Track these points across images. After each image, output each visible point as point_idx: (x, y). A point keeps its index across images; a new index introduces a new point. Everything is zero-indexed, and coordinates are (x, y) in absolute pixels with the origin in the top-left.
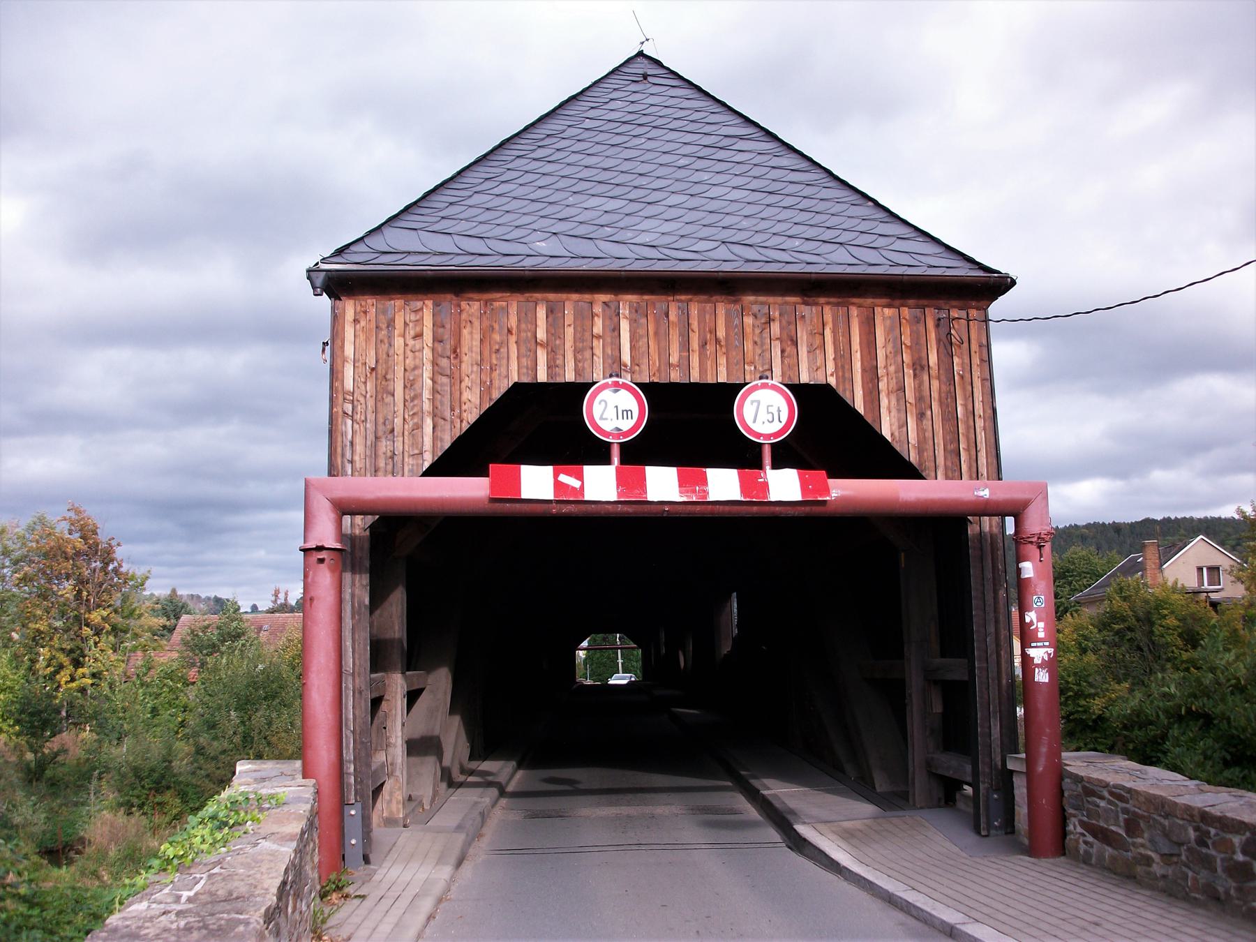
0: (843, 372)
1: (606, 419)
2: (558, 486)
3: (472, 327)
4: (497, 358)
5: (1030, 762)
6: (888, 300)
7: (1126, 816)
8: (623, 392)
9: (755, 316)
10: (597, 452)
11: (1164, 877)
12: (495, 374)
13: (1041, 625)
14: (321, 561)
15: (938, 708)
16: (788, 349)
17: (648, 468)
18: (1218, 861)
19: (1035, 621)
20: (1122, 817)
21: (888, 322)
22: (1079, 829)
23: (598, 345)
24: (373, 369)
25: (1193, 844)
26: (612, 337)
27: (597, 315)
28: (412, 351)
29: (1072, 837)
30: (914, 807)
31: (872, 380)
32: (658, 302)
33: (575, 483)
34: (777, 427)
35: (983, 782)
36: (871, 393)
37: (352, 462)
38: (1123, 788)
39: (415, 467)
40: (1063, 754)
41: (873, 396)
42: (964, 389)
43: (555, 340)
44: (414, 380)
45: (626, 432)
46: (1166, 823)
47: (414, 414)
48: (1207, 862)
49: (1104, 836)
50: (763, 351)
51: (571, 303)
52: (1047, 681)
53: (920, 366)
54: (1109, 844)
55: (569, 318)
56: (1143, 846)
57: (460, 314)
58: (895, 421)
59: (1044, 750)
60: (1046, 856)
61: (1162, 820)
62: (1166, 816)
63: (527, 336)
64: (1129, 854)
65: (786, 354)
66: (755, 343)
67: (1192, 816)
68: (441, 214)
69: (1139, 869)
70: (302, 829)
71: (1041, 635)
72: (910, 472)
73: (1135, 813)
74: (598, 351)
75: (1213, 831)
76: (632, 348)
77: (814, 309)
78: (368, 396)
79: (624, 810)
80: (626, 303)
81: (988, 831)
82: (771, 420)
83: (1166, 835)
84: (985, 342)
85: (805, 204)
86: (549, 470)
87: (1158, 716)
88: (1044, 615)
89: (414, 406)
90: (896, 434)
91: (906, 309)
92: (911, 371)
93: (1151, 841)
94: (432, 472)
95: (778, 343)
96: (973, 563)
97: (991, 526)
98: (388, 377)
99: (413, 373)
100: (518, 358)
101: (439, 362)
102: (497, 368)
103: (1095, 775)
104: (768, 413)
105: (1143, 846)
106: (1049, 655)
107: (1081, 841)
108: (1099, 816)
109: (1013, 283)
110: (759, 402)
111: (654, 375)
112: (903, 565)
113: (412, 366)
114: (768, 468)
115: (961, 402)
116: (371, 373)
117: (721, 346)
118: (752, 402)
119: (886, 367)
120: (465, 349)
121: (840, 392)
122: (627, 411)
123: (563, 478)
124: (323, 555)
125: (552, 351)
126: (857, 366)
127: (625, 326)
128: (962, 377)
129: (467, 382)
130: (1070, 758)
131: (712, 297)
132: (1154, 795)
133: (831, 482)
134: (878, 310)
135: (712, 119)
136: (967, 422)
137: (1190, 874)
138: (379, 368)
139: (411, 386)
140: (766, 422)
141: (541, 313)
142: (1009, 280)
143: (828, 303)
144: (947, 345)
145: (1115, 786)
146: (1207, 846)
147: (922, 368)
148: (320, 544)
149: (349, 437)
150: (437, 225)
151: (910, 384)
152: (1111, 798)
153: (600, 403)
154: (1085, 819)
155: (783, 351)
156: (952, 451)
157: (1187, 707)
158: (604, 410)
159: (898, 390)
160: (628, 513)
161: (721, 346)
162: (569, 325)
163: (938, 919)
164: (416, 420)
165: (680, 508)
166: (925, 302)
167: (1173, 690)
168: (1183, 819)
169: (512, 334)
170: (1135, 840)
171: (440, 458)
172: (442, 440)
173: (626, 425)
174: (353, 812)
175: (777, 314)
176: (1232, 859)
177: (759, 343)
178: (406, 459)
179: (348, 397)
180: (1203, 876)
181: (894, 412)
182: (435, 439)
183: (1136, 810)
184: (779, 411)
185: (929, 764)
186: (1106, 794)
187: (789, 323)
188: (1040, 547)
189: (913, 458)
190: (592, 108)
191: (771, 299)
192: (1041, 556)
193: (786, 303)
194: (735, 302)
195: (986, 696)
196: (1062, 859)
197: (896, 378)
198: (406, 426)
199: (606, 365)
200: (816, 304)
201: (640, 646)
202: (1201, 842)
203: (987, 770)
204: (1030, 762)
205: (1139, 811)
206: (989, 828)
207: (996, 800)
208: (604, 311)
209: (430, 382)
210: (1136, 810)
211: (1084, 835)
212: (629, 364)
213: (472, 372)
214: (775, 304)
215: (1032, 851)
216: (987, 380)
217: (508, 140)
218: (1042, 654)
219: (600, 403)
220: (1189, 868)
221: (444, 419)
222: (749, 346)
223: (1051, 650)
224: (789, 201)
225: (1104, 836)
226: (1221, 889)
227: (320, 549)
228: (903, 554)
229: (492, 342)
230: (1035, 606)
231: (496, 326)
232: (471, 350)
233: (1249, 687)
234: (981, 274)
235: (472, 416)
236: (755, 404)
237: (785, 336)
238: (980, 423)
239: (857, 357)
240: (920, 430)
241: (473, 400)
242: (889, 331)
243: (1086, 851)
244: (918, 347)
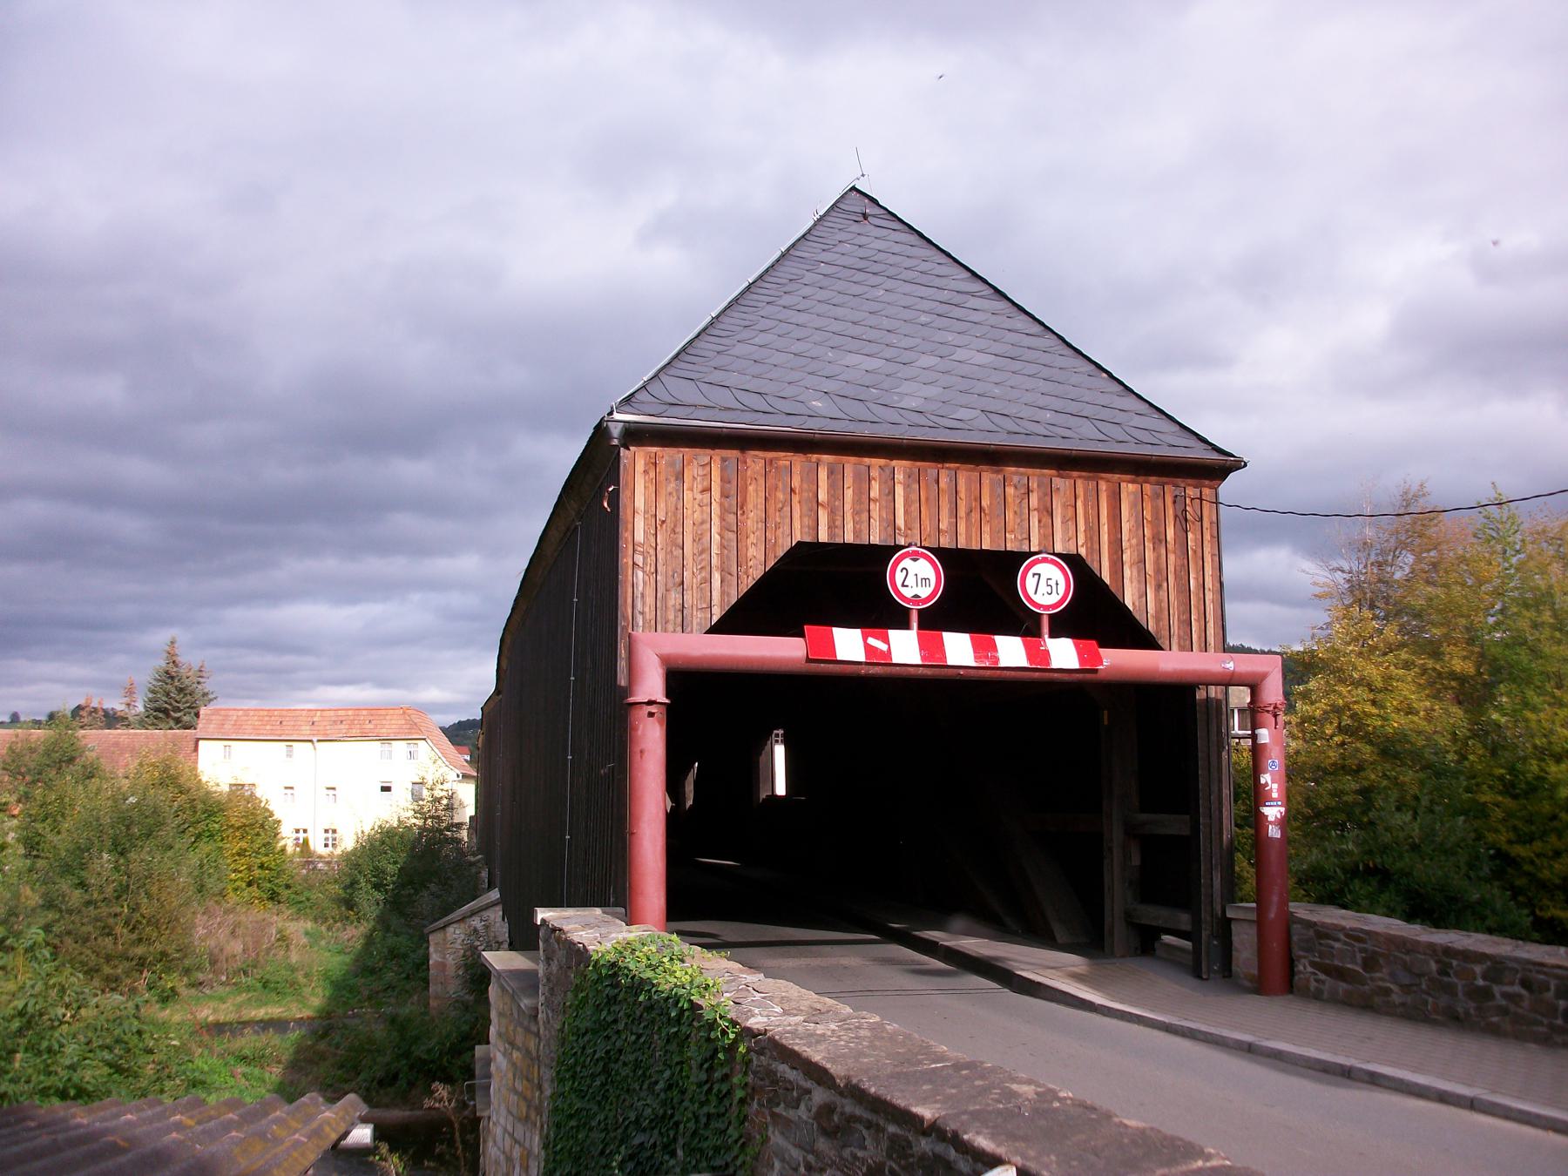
0: (1092, 544)
1: (907, 586)
2: (869, 649)
3: (757, 485)
4: (780, 517)
5: (1261, 910)
6: (1133, 477)
7: (1364, 955)
8: (922, 561)
9: (1016, 487)
10: (895, 616)
11: (1403, 1004)
12: (779, 532)
13: (1275, 786)
14: (651, 715)
15: (1136, 861)
16: (1044, 520)
18: (1460, 988)
19: (1269, 783)
20: (1359, 956)
21: (1132, 497)
22: (1309, 969)
23: (875, 508)
24: (663, 522)
25: (1435, 975)
26: (887, 501)
27: (874, 479)
28: (699, 505)
29: (1302, 976)
30: (1112, 955)
31: (1116, 553)
32: (930, 469)
33: (882, 646)
34: (1054, 599)
35: (1205, 930)
36: (1115, 563)
37: (642, 613)
38: (1362, 931)
39: (703, 622)
40: (1291, 904)
42: (1196, 563)
43: (835, 502)
44: (701, 534)
45: (927, 598)
46: (1407, 958)
47: (702, 568)
48: (1450, 990)
49: (1339, 974)
50: (1022, 521)
51: (850, 464)
52: (1279, 837)
53: (1159, 539)
54: (1344, 980)
55: (849, 481)
56: (1382, 979)
57: (746, 470)
58: (1135, 591)
59: (1275, 899)
60: (1276, 994)
61: (1404, 957)
62: (1408, 952)
63: (808, 496)
64: (1366, 987)
65: (1042, 524)
66: (1015, 512)
67: (1435, 951)
69: (1377, 1000)
71: (1275, 795)
72: (1145, 641)
73: (1375, 952)
74: (875, 514)
75: (1455, 963)
76: (906, 512)
77: (1067, 481)
78: (658, 548)
79: (803, 962)
80: (901, 467)
81: (1209, 975)
83: (1407, 968)
84: (1214, 519)
85: (1046, 372)
86: (858, 631)
87: (1335, 872)
88: (1277, 777)
89: (702, 560)
90: (1137, 604)
91: (1148, 485)
92: (1151, 545)
93: (1392, 975)
94: (715, 629)
95: (1036, 513)
96: (1201, 725)
97: (1216, 693)
98: (677, 530)
99: (701, 527)
100: (801, 517)
101: (726, 518)
102: (781, 525)
103: (1328, 920)
105: (1382, 979)
106: (1281, 813)
107: (1312, 980)
108: (1333, 956)
110: (1039, 575)
111: (925, 540)
112: (1106, 723)
113: (700, 521)
114: (1046, 636)
115: (1194, 576)
116: (661, 526)
117: (985, 514)
119: (1129, 540)
120: (750, 506)
121: (1089, 562)
123: (871, 641)
124: (653, 709)
125: (832, 511)
126: (1105, 538)
127: (899, 490)
128: (1195, 552)
129: (752, 539)
130: (1294, 907)
131: (978, 466)
132: (1394, 935)
133: (1102, 651)
134: (1123, 485)
136: (1198, 594)
137: (1430, 1000)
138: (668, 521)
139: (699, 540)
140: (1046, 594)
141: (823, 474)
143: (1080, 477)
144: (1182, 520)
145: (1352, 929)
146: (1450, 976)
147: (1160, 541)
148: (653, 699)
149: (641, 588)
151: (1150, 556)
152: (1347, 940)
153: (902, 571)
154: (1318, 960)
155: (1040, 521)
156: (1184, 621)
157: (1364, 864)
158: (905, 578)
159: (1138, 562)
160: (927, 676)
161: (985, 514)
162: (849, 488)
163: (1232, 1039)
164: (703, 574)
165: (972, 672)
166: (1165, 479)
167: (1351, 846)
168: (1425, 954)
169: (795, 493)
170: (1373, 975)
172: (728, 595)
173: (924, 592)
175: (1035, 485)
176: (1472, 984)
177: (1018, 512)
178: (695, 613)
179: (639, 549)
180: (1444, 1000)
181: (1135, 583)
182: (723, 593)
183: (1376, 949)
185: (1128, 916)
186: (1342, 937)
187: (1045, 495)
188: (1275, 716)
190: (824, 250)
191: (1030, 471)
192: (1276, 724)
193: (1044, 475)
194: (998, 472)
195: (1209, 850)
196: (1290, 996)
197: (1138, 550)
198: (695, 580)
199: (882, 528)
200: (1069, 477)
202: (1443, 972)
203: (1209, 919)
204: (1261, 910)
205: (1379, 950)
206: (1209, 973)
208: (880, 475)
210: (1376, 949)
211: (1316, 974)
213: (757, 528)
214: (1036, 477)
215: (1260, 987)
216: (1215, 555)
218: (1275, 813)
219: (902, 571)
220: (1429, 994)
221: (730, 574)
222: (1010, 515)
223: (1283, 809)
224: (1032, 369)
225: (1339, 974)
226: (1460, 1010)
227: (651, 703)
228: (1106, 712)
229: (777, 501)
230: (1270, 769)
231: (780, 485)
232: (756, 506)
233: (1422, 845)
234: (1215, 456)
235: (757, 573)
236: (1037, 577)
237: (1042, 507)
238: (1209, 596)
239: (1105, 529)
240: (1158, 601)
241: (758, 557)
242: (1133, 506)
243: (1317, 988)
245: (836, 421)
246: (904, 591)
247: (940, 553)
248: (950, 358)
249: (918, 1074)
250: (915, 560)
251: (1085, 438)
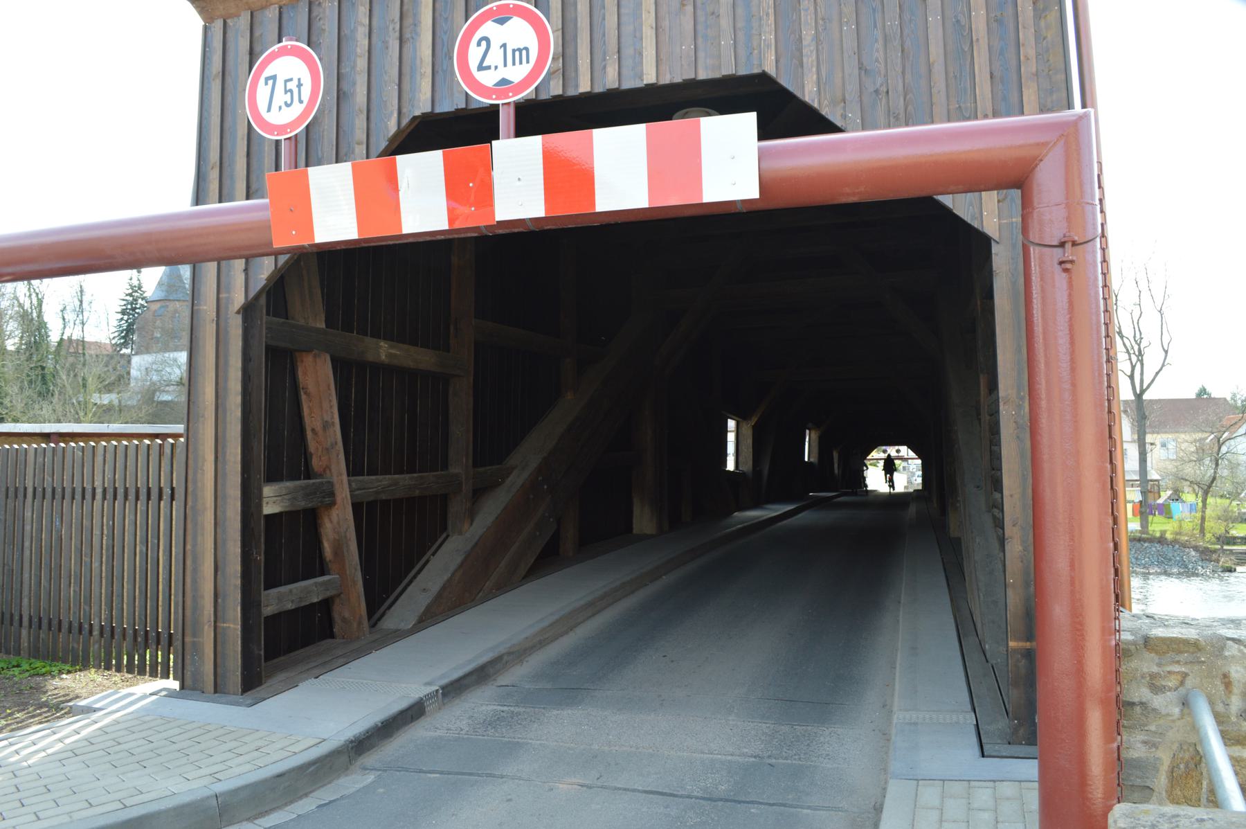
1: (489, 68)
17: (357, 237)
82: (289, 102)
104: (286, 92)
110: (274, 78)
122: (520, 50)
140: (283, 106)
153: (479, 44)
184: (300, 85)
201: (920, 457)
207: (475, 210)
219: (479, 44)
236: (270, 82)
249: (276, 133)
250: (502, 21)
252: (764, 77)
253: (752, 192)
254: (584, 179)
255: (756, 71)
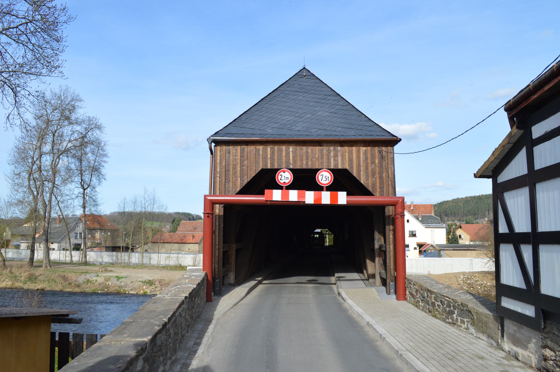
34: (327, 182)
35: (388, 279)
41: (359, 171)
68: (244, 122)
70: (199, 282)
72: (367, 193)
109: (400, 140)
110: (323, 175)
118: (321, 175)
135: (322, 89)
140: (325, 181)
141: (269, 149)
142: (399, 139)
144: (382, 157)
150: (242, 125)
171: (242, 189)
173: (287, 181)
174: (217, 281)
184: (328, 178)
189: (370, 189)
190: (288, 87)
195: (389, 255)
203: (389, 276)
209: (240, 168)
212: (292, 163)
217: (264, 98)
236: (322, 176)
244: (373, 156)
245: (479, 124)
246: (281, 181)
247: (331, 170)
248: (316, 114)
251: (351, 135)
252: (346, 169)
253: (346, 203)
254: (299, 196)
255: (345, 168)
